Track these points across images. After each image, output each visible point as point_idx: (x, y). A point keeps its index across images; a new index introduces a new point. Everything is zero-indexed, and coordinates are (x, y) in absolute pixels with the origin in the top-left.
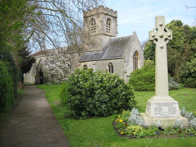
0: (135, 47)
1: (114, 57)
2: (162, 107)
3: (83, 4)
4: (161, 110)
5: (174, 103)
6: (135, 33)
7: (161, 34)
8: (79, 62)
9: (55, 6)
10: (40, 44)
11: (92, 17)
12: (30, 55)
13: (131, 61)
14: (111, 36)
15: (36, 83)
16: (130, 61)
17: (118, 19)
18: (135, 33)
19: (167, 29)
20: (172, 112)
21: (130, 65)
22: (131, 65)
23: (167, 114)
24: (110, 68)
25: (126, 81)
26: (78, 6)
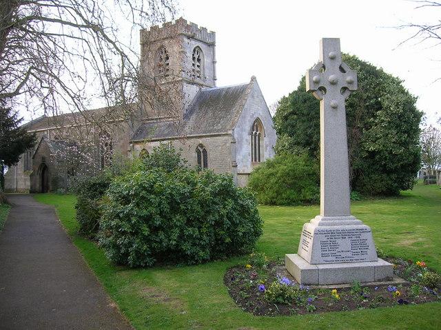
0: (251, 110)
1: (210, 132)
2: (337, 241)
3: (144, 14)
4: (335, 246)
5: (363, 231)
6: (253, 79)
7: (331, 77)
8: (131, 143)
9: (80, 15)
10: (44, 102)
11: (159, 44)
12: (19, 125)
13: (246, 140)
14: (202, 85)
15: (33, 191)
16: (244, 140)
17: (217, 48)
18: (253, 79)
19: (345, 67)
20: (359, 250)
21: (243, 149)
22: (246, 149)
23: (349, 254)
24: (199, 156)
25: (242, 183)
26: (131, 17)
